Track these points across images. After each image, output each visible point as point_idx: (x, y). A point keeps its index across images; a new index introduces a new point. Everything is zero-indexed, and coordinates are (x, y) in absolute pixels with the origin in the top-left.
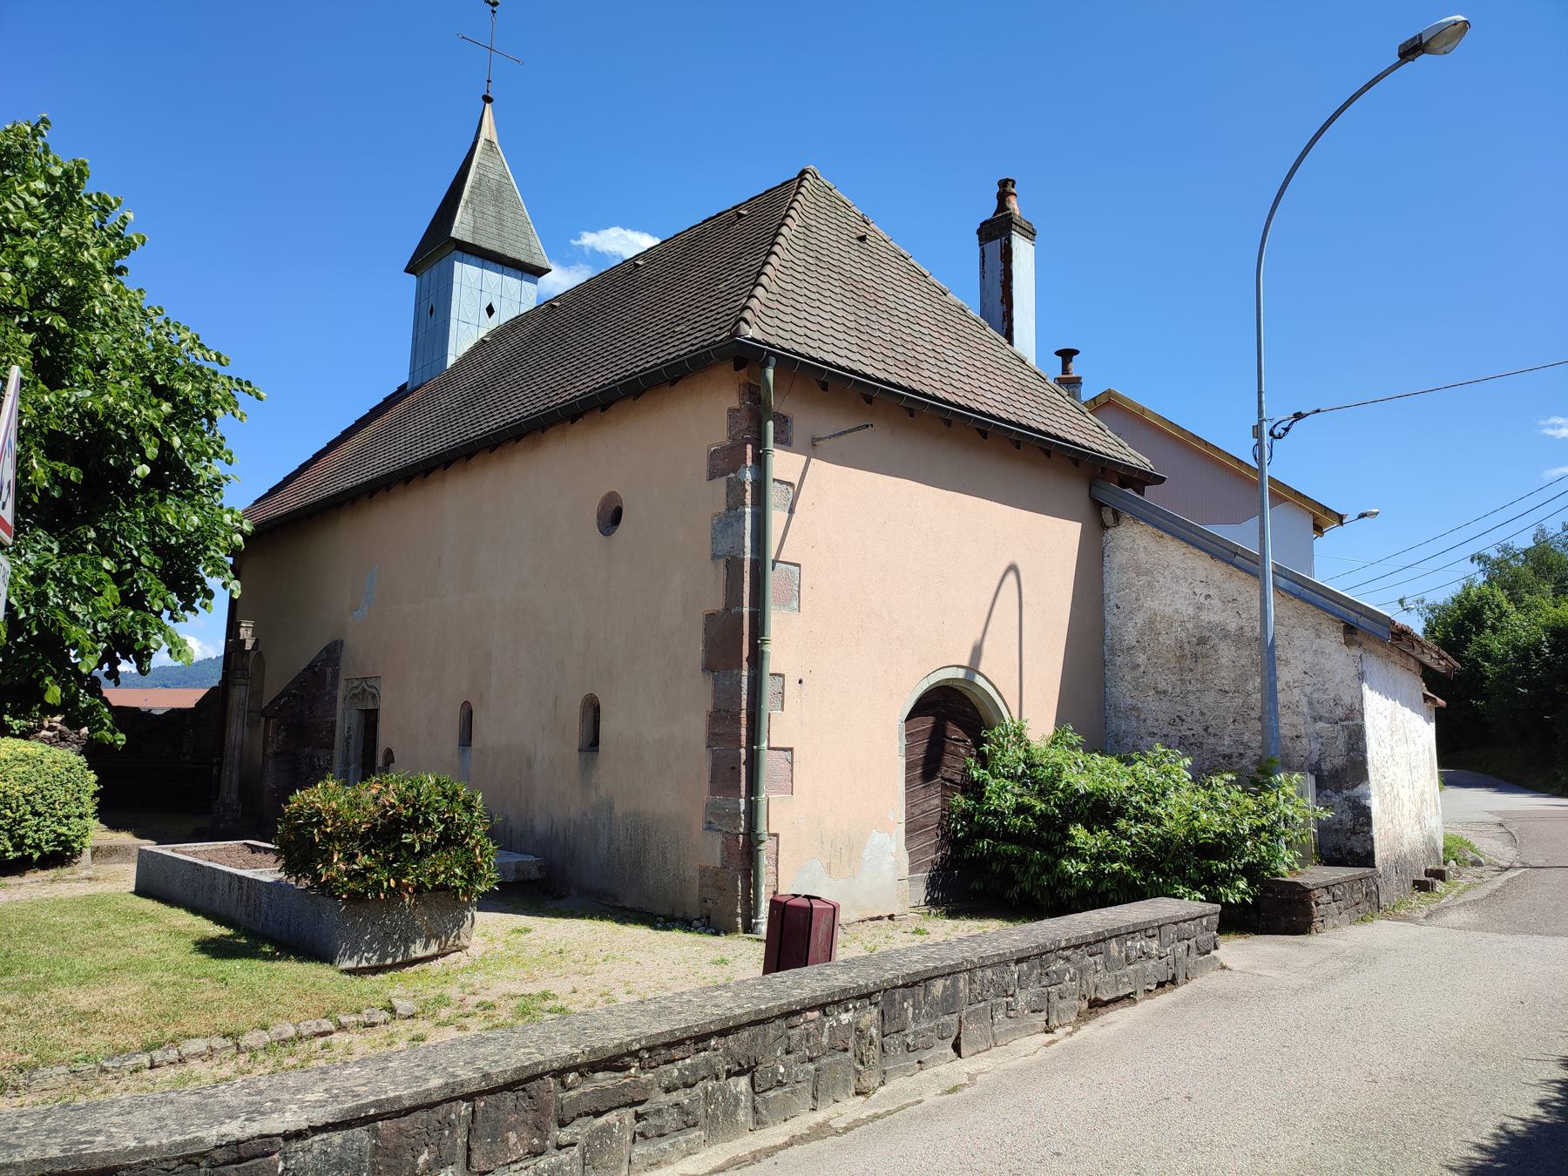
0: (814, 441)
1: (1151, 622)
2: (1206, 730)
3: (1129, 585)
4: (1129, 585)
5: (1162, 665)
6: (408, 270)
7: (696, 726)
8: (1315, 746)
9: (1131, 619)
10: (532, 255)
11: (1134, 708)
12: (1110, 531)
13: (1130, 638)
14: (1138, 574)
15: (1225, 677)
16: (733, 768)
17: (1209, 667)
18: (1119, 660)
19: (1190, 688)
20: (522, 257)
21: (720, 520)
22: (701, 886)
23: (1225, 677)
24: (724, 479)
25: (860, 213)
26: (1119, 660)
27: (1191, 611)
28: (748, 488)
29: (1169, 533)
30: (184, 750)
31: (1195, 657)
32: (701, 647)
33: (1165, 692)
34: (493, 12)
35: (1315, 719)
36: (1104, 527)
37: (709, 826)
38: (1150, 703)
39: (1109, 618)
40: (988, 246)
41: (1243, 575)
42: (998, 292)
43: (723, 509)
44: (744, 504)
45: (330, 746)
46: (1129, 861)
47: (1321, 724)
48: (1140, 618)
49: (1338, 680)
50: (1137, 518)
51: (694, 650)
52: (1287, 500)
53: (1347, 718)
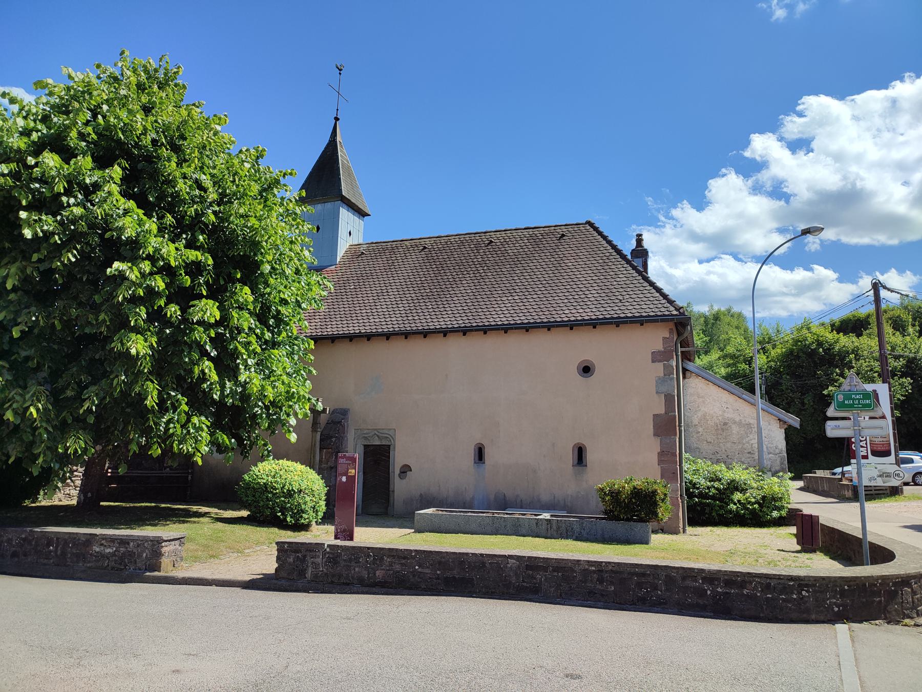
1: (704, 416)
2: (727, 456)
5: (709, 432)
8: (769, 463)
11: (697, 448)
13: (696, 421)
21: (660, 379)
24: (662, 363)
30: (165, 465)
31: (723, 430)
32: (652, 427)
33: (710, 442)
35: (769, 454)
47: (771, 455)
48: (699, 414)
53: (780, 453)
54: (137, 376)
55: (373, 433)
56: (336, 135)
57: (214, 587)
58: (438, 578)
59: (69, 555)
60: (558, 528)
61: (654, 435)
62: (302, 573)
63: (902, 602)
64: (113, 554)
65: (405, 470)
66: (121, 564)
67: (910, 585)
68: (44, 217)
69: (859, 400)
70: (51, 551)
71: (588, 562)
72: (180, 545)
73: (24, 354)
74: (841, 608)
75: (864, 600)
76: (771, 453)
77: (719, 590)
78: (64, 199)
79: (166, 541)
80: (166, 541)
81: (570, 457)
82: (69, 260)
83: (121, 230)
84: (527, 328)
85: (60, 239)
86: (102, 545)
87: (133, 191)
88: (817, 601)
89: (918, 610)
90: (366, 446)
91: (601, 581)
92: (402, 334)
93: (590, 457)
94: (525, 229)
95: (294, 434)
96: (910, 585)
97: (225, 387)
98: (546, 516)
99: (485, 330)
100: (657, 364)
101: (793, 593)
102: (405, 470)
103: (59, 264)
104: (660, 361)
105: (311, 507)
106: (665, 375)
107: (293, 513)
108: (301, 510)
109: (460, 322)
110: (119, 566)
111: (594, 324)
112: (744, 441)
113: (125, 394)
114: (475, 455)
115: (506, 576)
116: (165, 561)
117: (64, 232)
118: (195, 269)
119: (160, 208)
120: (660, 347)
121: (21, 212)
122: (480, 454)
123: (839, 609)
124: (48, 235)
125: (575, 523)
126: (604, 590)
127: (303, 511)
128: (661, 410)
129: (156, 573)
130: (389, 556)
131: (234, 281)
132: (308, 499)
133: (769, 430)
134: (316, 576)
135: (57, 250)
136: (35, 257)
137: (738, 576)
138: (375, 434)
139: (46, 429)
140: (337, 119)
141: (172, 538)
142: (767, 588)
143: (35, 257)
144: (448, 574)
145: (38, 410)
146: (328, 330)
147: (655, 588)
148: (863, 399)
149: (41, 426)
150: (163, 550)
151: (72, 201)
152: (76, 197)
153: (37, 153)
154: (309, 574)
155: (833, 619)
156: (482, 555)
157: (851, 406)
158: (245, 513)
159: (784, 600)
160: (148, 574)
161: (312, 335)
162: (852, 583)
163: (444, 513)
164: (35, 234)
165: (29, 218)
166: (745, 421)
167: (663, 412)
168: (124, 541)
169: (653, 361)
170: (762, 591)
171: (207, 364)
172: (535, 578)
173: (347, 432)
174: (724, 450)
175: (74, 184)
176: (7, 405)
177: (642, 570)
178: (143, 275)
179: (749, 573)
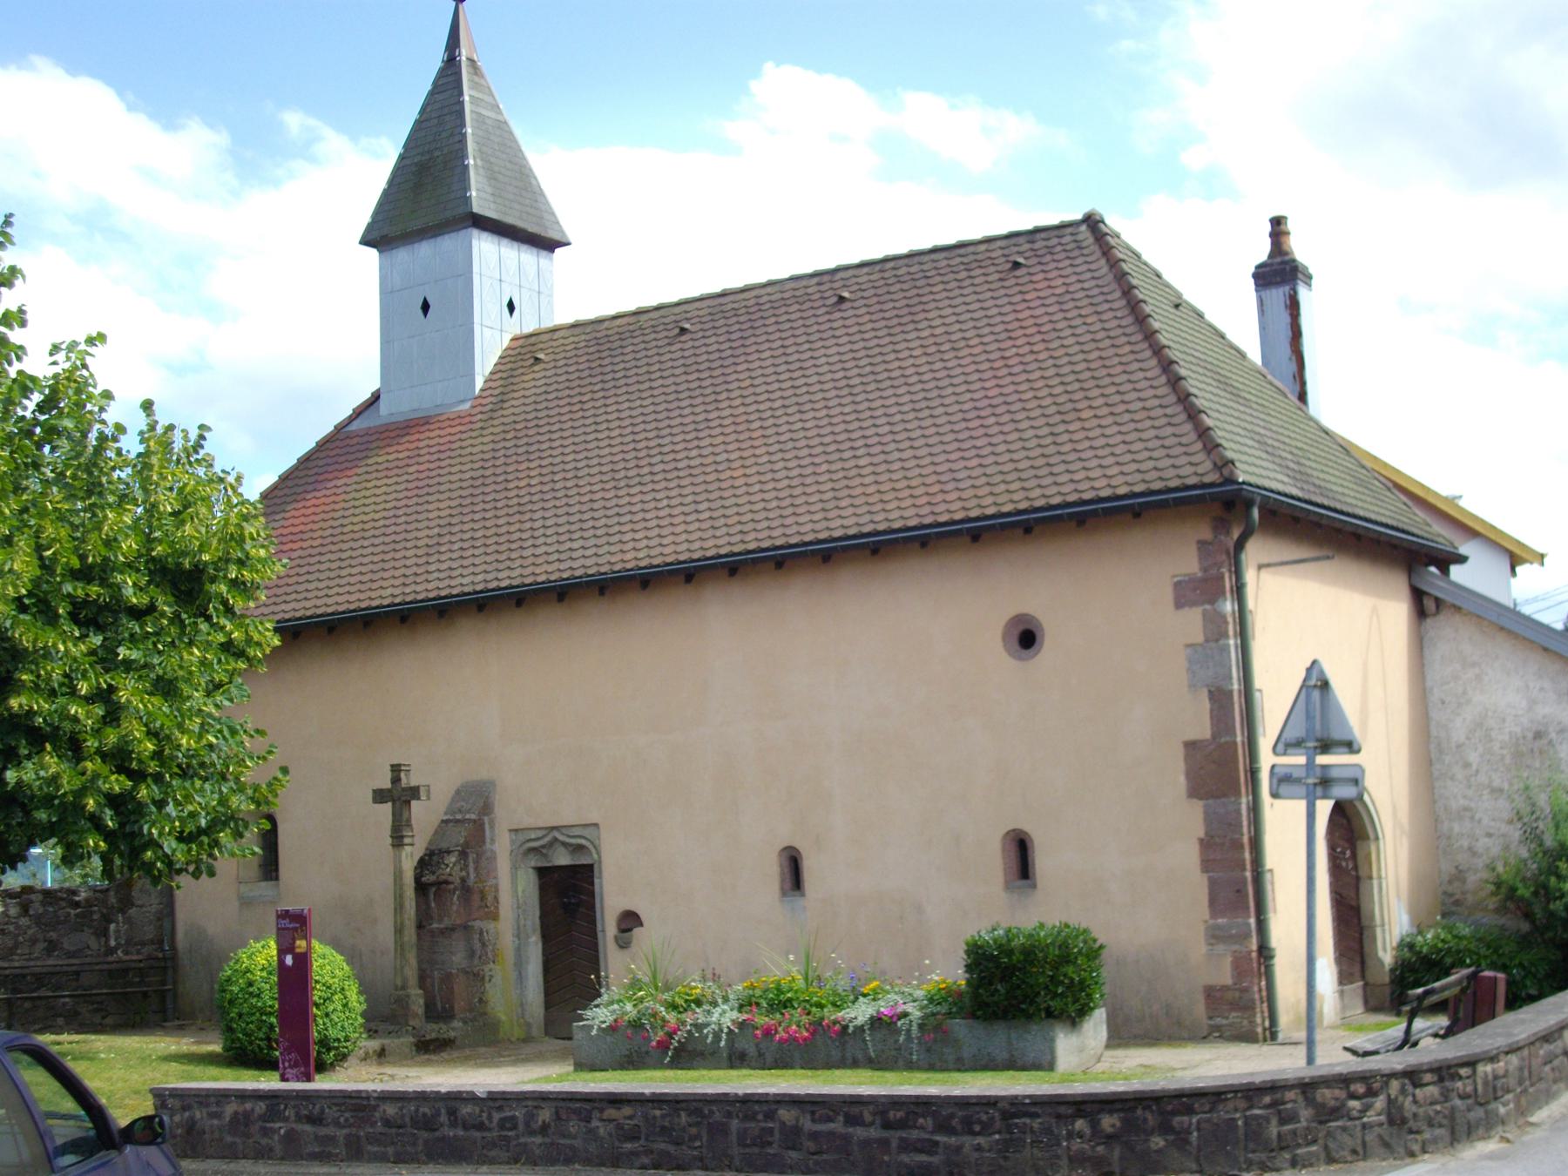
6: (367, 241)
7: (1186, 855)
9: (1459, 715)
11: (1466, 809)
16: (1238, 891)
20: (532, 228)
28: (1230, 620)
33: (1501, 790)
40: (1268, 294)
44: (1226, 636)
45: (495, 917)
65: (630, 921)
81: (995, 861)
89: (1296, 1155)
90: (542, 872)
93: (1042, 862)
100: (389, 775)
104: (1193, 604)
122: (793, 871)
128: (1201, 729)
138: (556, 839)
158: (216, 1048)
173: (493, 840)
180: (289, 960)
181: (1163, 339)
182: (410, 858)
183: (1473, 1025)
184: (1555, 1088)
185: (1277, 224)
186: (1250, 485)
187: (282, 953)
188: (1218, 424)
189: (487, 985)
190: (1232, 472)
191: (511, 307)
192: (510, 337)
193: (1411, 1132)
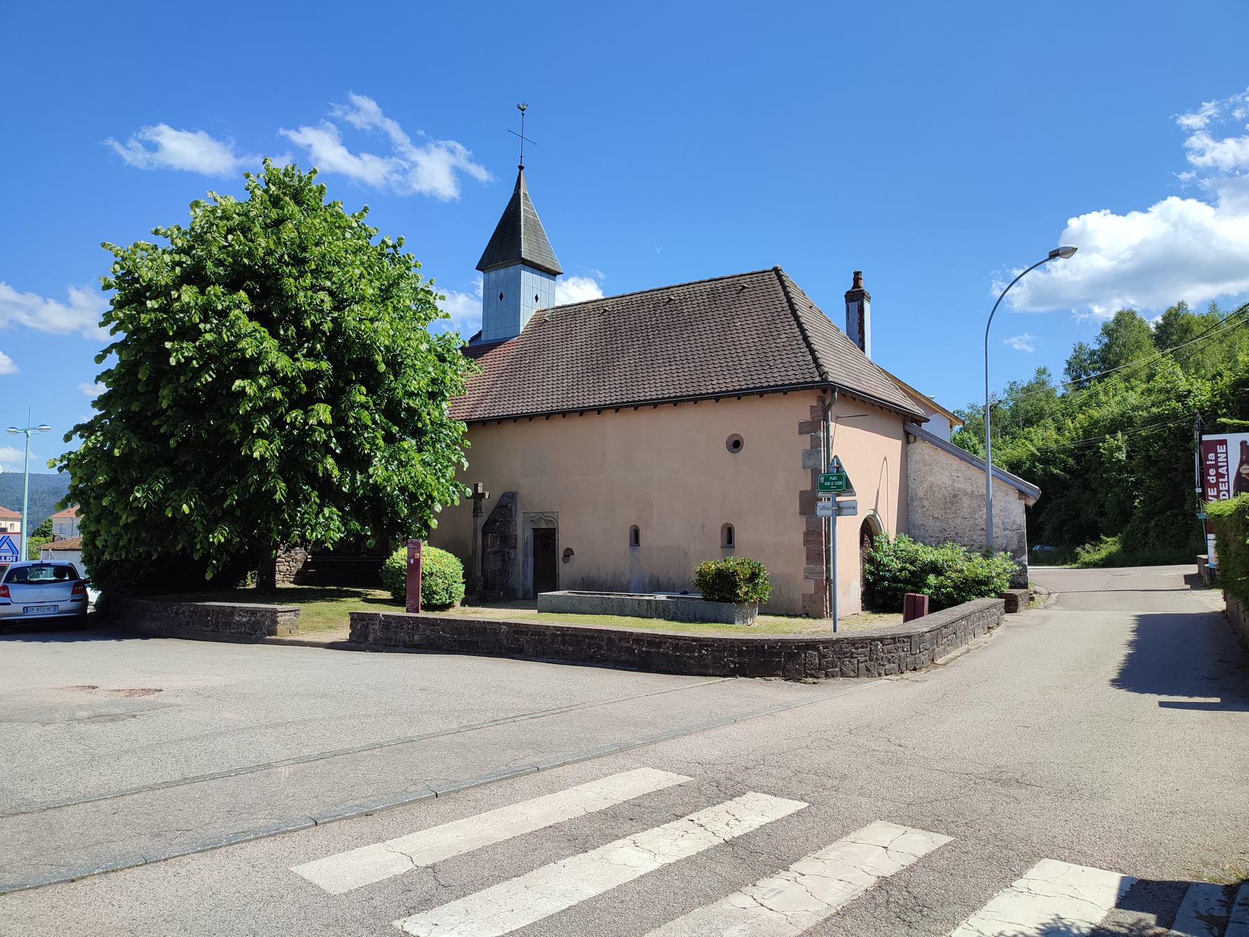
0: (837, 417)
1: (931, 487)
2: (957, 534)
3: (920, 470)
4: (920, 470)
6: (478, 268)
10: (554, 265)
12: (911, 445)
13: (921, 494)
14: (924, 465)
15: (965, 511)
17: (958, 508)
18: (915, 504)
19: (949, 516)
22: (803, 601)
23: (965, 511)
24: (809, 435)
25: (801, 290)
26: (915, 504)
27: (950, 483)
29: (941, 448)
31: (952, 503)
32: (798, 505)
33: (938, 518)
34: (523, 114)
35: (1005, 530)
36: (908, 442)
37: (806, 577)
38: (930, 523)
39: (910, 485)
40: (851, 304)
41: (974, 468)
42: (857, 328)
43: (809, 448)
45: (515, 547)
46: (952, 587)
48: (925, 485)
49: (1014, 514)
50: (924, 440)
51: (796, 505)
52: (938, 412)
53: (1018, 529)
54: (265, 475)
55: (539, 517)
56: (520, 187)
57: (308, 648)
58: (455, 641)
59: (220, 624)
60: (657, 608)
61: (800, 514)
62: (366, 637)
63: (805, 664)
64: (247, 622)
66: (252, 630)
67: (817, 649)
68: (184, 345)
69: (834, 481)
70: (209, 621)
71: (555, 627)
72: (295, 616)
73: (183, 459)
74: (737, 665)
75: (762, 659)
76: (1007, 529)
77: (644, 649)
78: (202, 326)
79: (281, 612)
80: (281, 612)
81: (718, 538)
82: (206, 380)
83: (243, 350)
84: (676, 402)
85: (198, 363)
86: (240, 615)
87: (262, 308)
88: (714, 659)
90: (535, 530)
91: (564, 643)
92: (559, 413)
93: (737, 538)
94: (709, 281)
95: (435, 520)
96: (817, 649)
97: (356, 479)
98: (662, 597)
99: (636, 406)
100: (804, 436)
101: (695, 652)
102: (569, 553)
103: (199, 384)
105: (444, 589)
106: (812, 448)
107: (425, 594)
108: (433, 591)
109: (613, 398)
110: (250, 632)
111: (739, 395)
112: (977, 516)
113: (258, 490)
114: (631, 537)
115: (500, 639)
116: (280, 628)
117: (201, 357)
118: (312, 377)
119: (286, 321)
120: (807, 417)
121: (166, 343)
123: (735, 666)
124: (189, 360)
125: (671, 603)
126: (565, 650)
127: (435, 593)
129: (274, 637)
130: (423, 624)
131: (351, 381)
132: (440, 581)
133: (1006, 502)
134: (375, 639)
135: (197, 373)
136: (182, 379)
137: (657, 638)
139: (201, 522)
140: (521, 168)
141: (286, 610)
142: (676, 647)
143: (182, 379)
144: (462, 638)
145: (190, 507)
146: (495, 411)
147: (600, 648)
148: (837, 481)
149: (197, 520)
150: (278, 619)
151: (208, 326)
152: (211, 323)
153: (177, 287)
154: (371, 639)
155: (729, 674)
156: (484, 622)
157: (829, 487)
159: (688, 657)
160: (268, 637)
161: (466, 419)
162: (749, 645)
163: (618, 597)
164: (178, 361)
165: (173, 346)
166: (978, 491)
167: (810, 488)
168: (253, 612)
169: (801, 433)
170: (673, 649)
171: (330, 462)
172: (520, 641)
173: (516, 516)
174: (953, 528)
175: (207, 311)
176: (167, 504)
177: (592, 634)
178: (260, 388)
179: (663, 635)
180: (412, 561)
181: (802, 320)
182: (481, 521)
183: (914, 618)
184: (948, 649)
185: (857, 274)
186: (835, 383)
187: (409, 558)
188: (823, 356)
189: (510, 576)
190: (826, 377)
191: (537, 298)
192: (536, 310)
193: (880, 665)
